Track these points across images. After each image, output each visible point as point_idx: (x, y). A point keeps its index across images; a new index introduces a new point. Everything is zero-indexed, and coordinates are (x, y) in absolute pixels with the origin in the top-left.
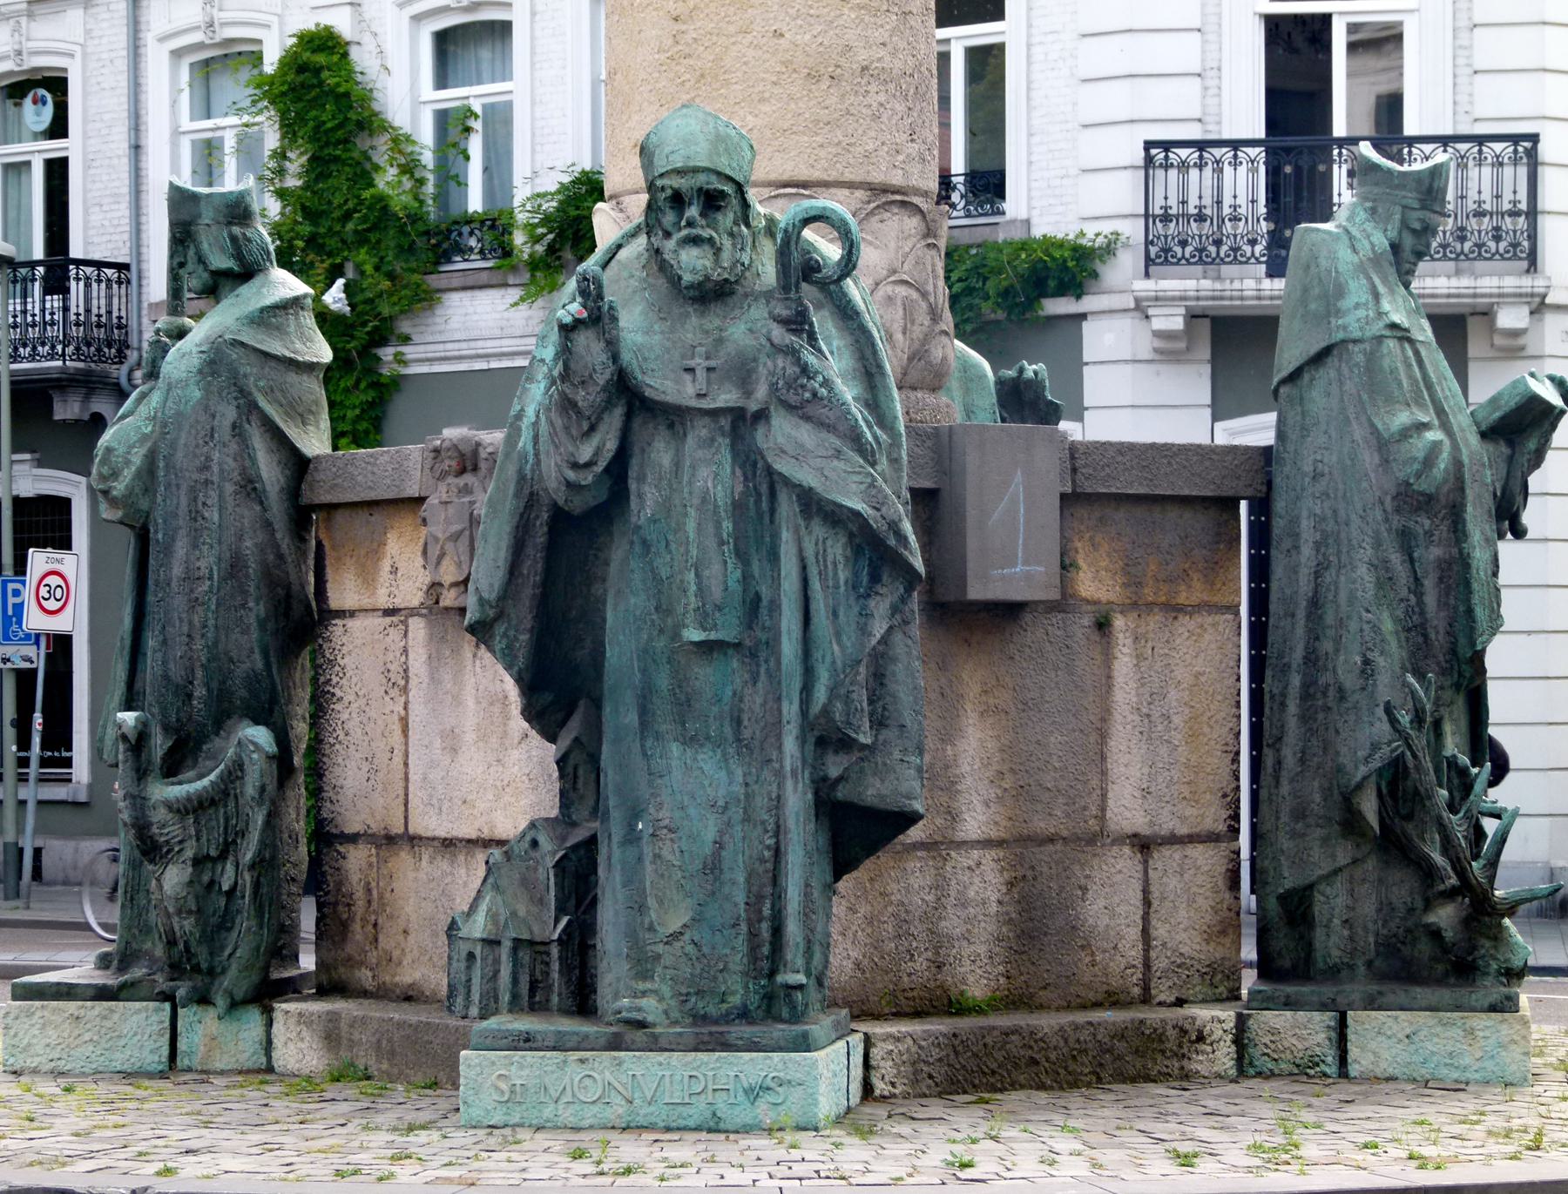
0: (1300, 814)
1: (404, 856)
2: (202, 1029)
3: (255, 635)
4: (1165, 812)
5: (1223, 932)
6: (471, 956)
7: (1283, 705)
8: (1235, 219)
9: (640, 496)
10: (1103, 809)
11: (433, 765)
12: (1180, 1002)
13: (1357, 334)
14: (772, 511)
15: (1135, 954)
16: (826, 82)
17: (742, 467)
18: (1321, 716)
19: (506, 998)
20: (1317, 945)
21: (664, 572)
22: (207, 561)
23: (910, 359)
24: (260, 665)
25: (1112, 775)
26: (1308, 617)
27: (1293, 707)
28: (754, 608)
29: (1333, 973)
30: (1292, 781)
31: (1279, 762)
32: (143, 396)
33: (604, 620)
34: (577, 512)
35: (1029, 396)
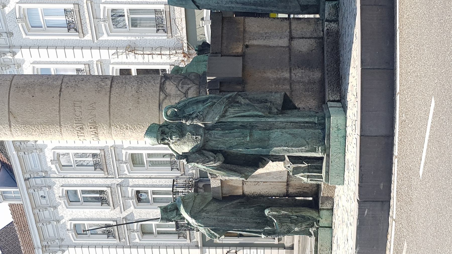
1: (291, 183)
2: (323, 222)
3: (247, 209)
4: (285, 34)
5: (309, 22)
10: (284, 47)
12: (323, 31)
14: (224, 122)
15: (313, 40)
16: (139, 100)
17: (215, 128)
18: (266, 3)
19: (319, 174)
21: (236, 144)
22: (233, 219)
23: (194, 83)
24: (253, 209)
28: (243, 126)
30: (279, 9)
34: (224, 159)
35: (201, 48)
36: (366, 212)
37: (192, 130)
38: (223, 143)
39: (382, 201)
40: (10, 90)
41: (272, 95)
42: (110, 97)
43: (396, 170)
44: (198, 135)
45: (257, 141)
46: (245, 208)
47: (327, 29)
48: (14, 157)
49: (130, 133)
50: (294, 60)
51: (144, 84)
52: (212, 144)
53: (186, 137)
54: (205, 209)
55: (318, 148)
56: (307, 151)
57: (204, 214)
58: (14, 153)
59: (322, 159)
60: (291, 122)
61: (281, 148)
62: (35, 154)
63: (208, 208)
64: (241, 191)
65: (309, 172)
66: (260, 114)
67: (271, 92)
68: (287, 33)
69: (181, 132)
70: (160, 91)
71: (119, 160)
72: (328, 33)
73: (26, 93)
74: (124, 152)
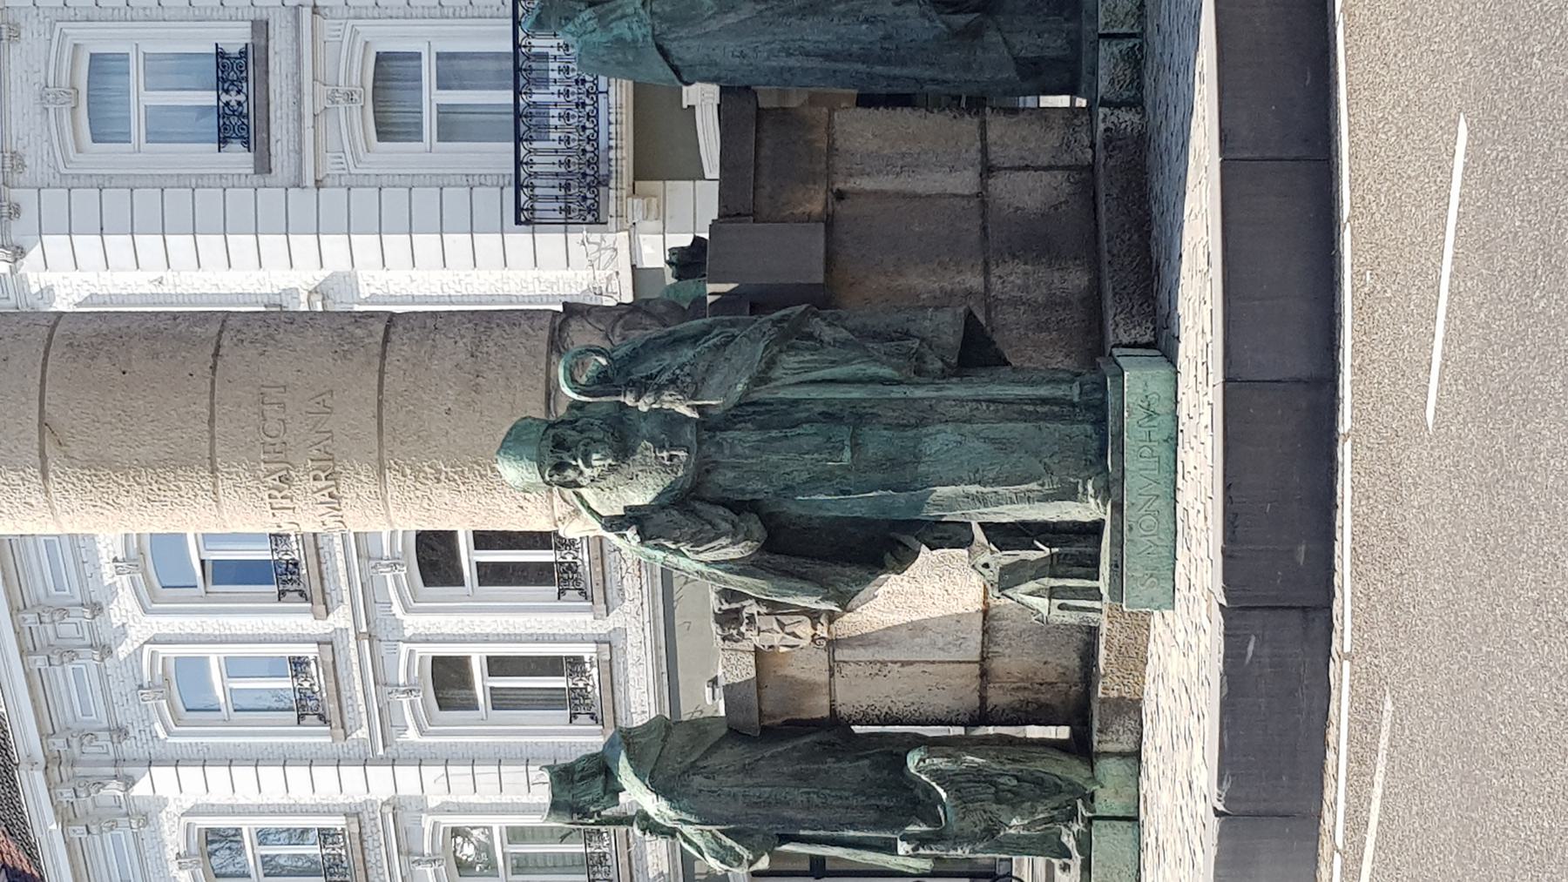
0: (967, 67)
1: (997, 665)
2: (1108, 801)
3: (846, 765)
6: (1060, 607)
7: (895, 78)
8: (568, 140)
9: (755, 492)
10: (963, 196)
11: (933, 644)
12: (1092, 146)
13: (649, 29)
14: (765, 404)
15: (1060, 175)
18: (902, 52)
19: (1088, 583)
20: (1054, 54)
21: (805, 476)
22: (798, 795)
24: (866, 762)
25: (940, 190)
26: (836, 61)
27: (897, 71)
28: (830, 416)
29: (1075, 43)
31: (933, 80)
32: (686, 840)
33: (837, 518)
35: (688, 259)
36: (1251, 648)
37: (656, 431)
38: (764, 475)
39: (1304, 608)
40: (46, 353)
41: (925, 318)
42: (381, 373)
43: (1348, 484)
44: (679, 447)
45: (879, 466)
46: (839, 760)
47: (1106, 130)
48: (51, 846)
49: (447, 498)
50: (998, 236)
51: (497, 332)
52: (725, 478)
53: (638, 457)
54: (701, 764)
55: (1085, 484)
56: (1046, 498)
57: (698, 781)
58: (54, 827)
59: (1095, 528)
60: (989, 401)
61: (961, 489)
62: (124, 833)
63: (714, 761)
64: (825, 701)
65: (1056, 577)
66: (886, 372)
67: (924, 308)
68: (974, 154)
69: (620, 439)
70: (550, 353)
71: (409, 853)
72: (1108, 142)
73: (103, 361)
74: (427, 822)
